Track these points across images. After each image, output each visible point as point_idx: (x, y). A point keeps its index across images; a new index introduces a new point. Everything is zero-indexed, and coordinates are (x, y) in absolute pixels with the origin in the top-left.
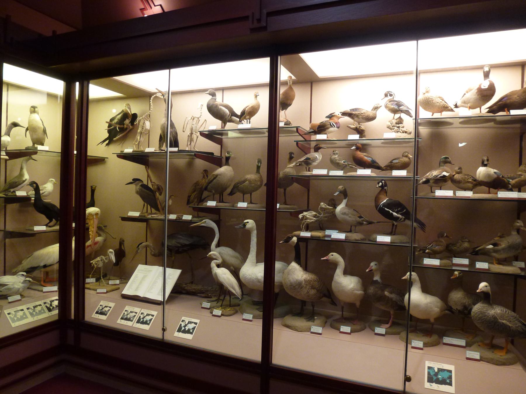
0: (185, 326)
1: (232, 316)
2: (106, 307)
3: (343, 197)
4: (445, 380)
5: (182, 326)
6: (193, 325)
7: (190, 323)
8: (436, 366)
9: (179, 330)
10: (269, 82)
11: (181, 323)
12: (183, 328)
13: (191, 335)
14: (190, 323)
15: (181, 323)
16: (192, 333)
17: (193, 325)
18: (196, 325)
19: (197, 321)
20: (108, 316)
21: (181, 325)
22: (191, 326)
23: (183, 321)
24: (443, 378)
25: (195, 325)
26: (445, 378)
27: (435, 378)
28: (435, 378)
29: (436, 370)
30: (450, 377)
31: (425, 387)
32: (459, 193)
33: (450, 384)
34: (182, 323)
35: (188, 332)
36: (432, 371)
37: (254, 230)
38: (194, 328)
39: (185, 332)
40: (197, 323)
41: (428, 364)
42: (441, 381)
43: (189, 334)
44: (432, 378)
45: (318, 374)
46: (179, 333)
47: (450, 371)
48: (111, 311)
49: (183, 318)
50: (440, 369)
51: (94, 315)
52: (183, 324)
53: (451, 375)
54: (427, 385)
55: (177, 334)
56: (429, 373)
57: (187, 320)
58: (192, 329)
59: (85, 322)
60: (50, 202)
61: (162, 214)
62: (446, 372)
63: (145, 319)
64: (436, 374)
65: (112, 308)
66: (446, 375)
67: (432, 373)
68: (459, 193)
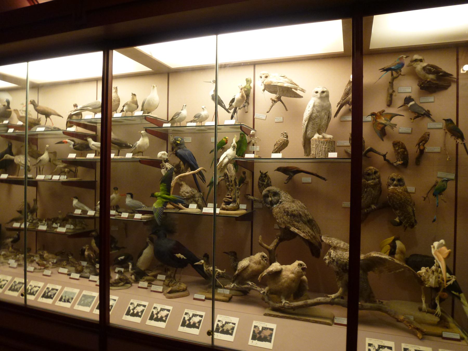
0: (157, 314)
1: (187, 297)
2: (35, 287)
3: (159, 169)
4: (267, 337)
5: (131, 308)
6: (165, 313)
7: (162, 310)
8: (261, 325)
9: (183, 324)
10: (102, 77)
11: (153, 310)
12: (155, 316)
13: (198, 329)
14: (162, 310)
15: (129, 305)
16: (164, 321)
17: (165, 313)
18: (169, 312)
19: (170, 308)
20: (167, 323)
21: (184, 318)
22: (164, 313)
23: (132, 304)
24: (227, 329)
25: (168, 312)
26: (267, 336)
27: (258, 336)
28: (258, 336)
29: (260, 329)
30: (271, 335)
31: (249, 344)
32: (340, 143)
33: (270, 341)
34: (185, 316)
35: (161, 320)
36: (257, 330)
37: (98, 205)
38: (167, 316)
39: (190, 326)
40: (95, 297)
41: (255, 323)
42: (226, 331)
43: (267, 342)
44: (256, 336)
45: (47, 310)
46: (184, 327)
47: (272, 330)
48: (251, 328)
49: (186, 311)
50: (264, 328)
51: (58, 303)
52: (132, 307)
53: (272, 333)
54: (251, 342)
55: (181, 329)
56: (254, 331)
57: (191, 313)
58: (269, 336)
59: (215, 348)
60: (80, 180)
61: (400, 160)
62: (386, 349)
63: (16, 287)
64: (260, 332)
65: (41, 288)
66: (267, 333)
67: (257, 331)
68: (340, 143)
